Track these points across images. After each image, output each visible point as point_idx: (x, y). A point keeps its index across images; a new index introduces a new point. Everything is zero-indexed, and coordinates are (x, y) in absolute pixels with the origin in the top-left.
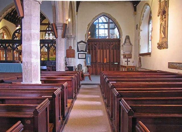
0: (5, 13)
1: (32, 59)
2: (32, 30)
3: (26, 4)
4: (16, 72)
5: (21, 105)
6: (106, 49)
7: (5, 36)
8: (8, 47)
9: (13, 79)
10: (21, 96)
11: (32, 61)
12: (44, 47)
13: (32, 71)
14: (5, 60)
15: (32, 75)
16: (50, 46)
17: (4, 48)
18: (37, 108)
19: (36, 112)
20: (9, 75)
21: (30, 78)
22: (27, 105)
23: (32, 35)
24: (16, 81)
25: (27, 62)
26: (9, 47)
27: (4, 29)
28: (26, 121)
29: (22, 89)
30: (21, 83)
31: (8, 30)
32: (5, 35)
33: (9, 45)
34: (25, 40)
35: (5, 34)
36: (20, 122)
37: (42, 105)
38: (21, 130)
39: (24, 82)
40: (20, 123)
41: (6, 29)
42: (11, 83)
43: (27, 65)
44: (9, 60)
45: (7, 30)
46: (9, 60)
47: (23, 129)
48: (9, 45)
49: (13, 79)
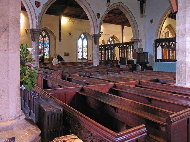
0: (169, 11)
1: (187, 58)
2: (187, 25)
3: (180, 2)
4: (157, 70)
5: (164, 110)
6: (103, 50)
7: (170, 35)
8: (171, 45)
9: (169, 79)
10: (174, 100)
11: (187, 61)
12: (159, 46)
13: (187, 72)
14: (167, 59)
15: (186, 76)
16: (170, 44)
17: (167, 47)
18: (171, 116)
19: (169, 121)
20: (167, 75)
21: (184, 80)
22: (163, 110)
23: (187, 30)
24: (170, 81)
25: (181, 62)
26: (173, 46)
27: (169, 28)
28: (161, 127)
29: (184, 93)
30: (175, 84)
31: (172, 28)
32: (169, 34)
33: (173, 43)
34: (178, 36)
35: (169, 32)
36: (144, 125)
37: (179, 115)
38: (143, 135)
39: (177, 84)
40: (143, 127)
41: (170, 28)
42: (165, 83)
43: (181, 64)
44: (173, 59)
45: (171, 29)
46: (173, 59)
47: (146, 134)
48: (173, 43)
49: (169, 79)
